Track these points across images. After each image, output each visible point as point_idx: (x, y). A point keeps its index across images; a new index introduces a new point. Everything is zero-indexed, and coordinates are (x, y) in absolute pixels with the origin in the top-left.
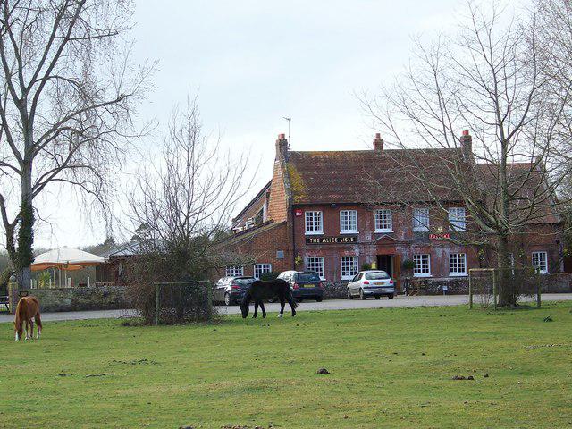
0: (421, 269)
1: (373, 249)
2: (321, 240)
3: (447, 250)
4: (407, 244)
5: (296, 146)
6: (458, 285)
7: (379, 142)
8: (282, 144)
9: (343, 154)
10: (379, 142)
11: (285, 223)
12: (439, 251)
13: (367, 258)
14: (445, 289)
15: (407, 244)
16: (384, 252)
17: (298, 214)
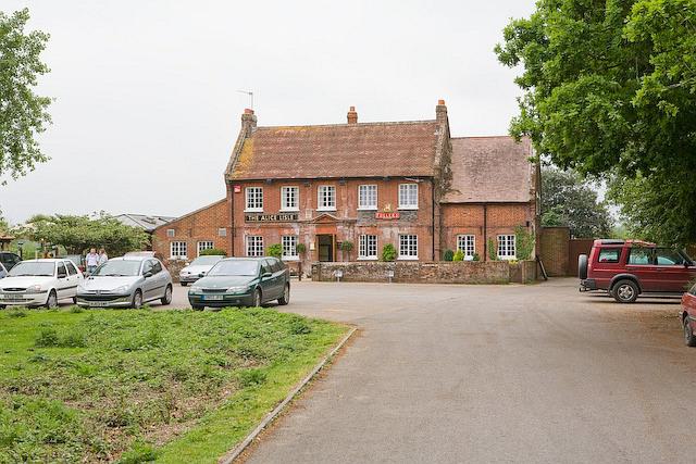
0: (507, 251)
1: (312, 229)
2: (260, 218)
3: (396, 231)
4: (351, 223)
5: (264, 121)
6: (357, 271)
7: (352, 117)
8: (249, 119)
9: (309, 128)
10: (352, 117)
11: (225, 201)
12: (387, 231)
13: (307, 238)
14: (340, 275)
15: (351, 223)
16: (324, 231)
17: (237, 190)
